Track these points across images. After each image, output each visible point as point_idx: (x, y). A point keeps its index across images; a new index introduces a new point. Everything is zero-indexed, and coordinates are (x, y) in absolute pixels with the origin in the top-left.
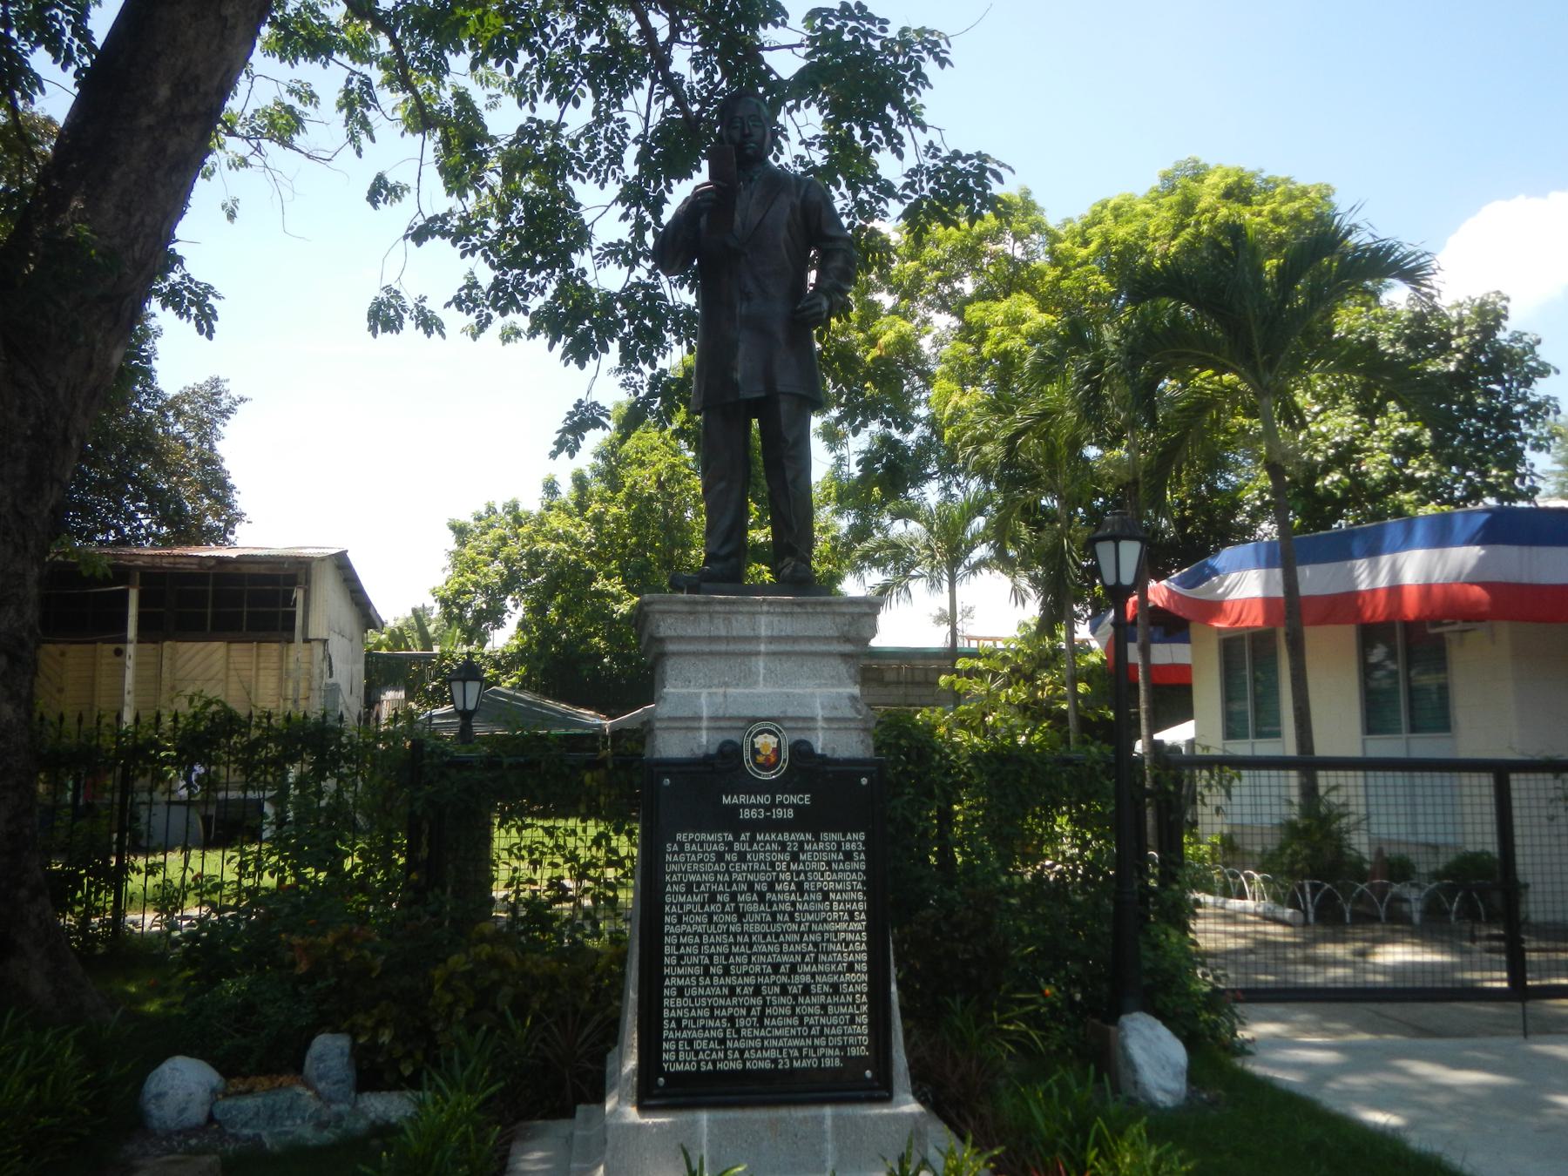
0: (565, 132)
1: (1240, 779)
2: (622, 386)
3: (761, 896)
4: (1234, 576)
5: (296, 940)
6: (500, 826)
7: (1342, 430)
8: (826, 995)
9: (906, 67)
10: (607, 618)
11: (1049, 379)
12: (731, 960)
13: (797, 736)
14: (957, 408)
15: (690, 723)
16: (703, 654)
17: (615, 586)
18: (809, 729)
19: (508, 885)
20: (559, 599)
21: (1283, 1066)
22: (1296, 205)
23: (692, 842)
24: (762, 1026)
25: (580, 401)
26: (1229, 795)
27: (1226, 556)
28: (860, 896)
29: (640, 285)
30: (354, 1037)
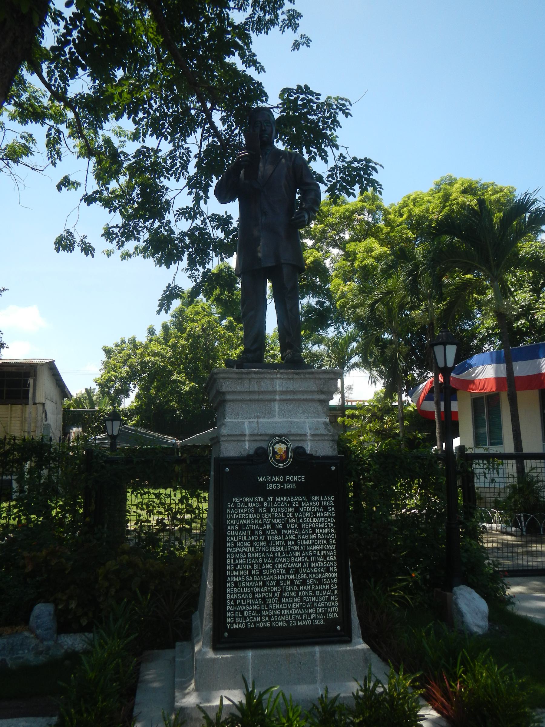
0: (160, 154)
1: (502, 464)
2: (189, 277)
3: (279, 531)
4: (480, 368)
5: (26, 554)
6: (132, 493)
7: (525, 299)
8: (315, 585)
9: (329, 118)
10: (179, 393)
11: (390, 276)
12: (264, 567)
13: (297, 444)
14: (342, 292)
15: (239, 437)
16: (246, 400)
17: (182, 377)
18: (303, 440)
19: (136, 524)
20: (155, 384)
21: (531, 610)
22: (498, 196)
23: (241, 502)
24: (281, 603)
25: (169, 285)
26: (498, 473)
27: (474, 360)
28: (332, 531)
29: (197, 228)
30: (56, 605)
